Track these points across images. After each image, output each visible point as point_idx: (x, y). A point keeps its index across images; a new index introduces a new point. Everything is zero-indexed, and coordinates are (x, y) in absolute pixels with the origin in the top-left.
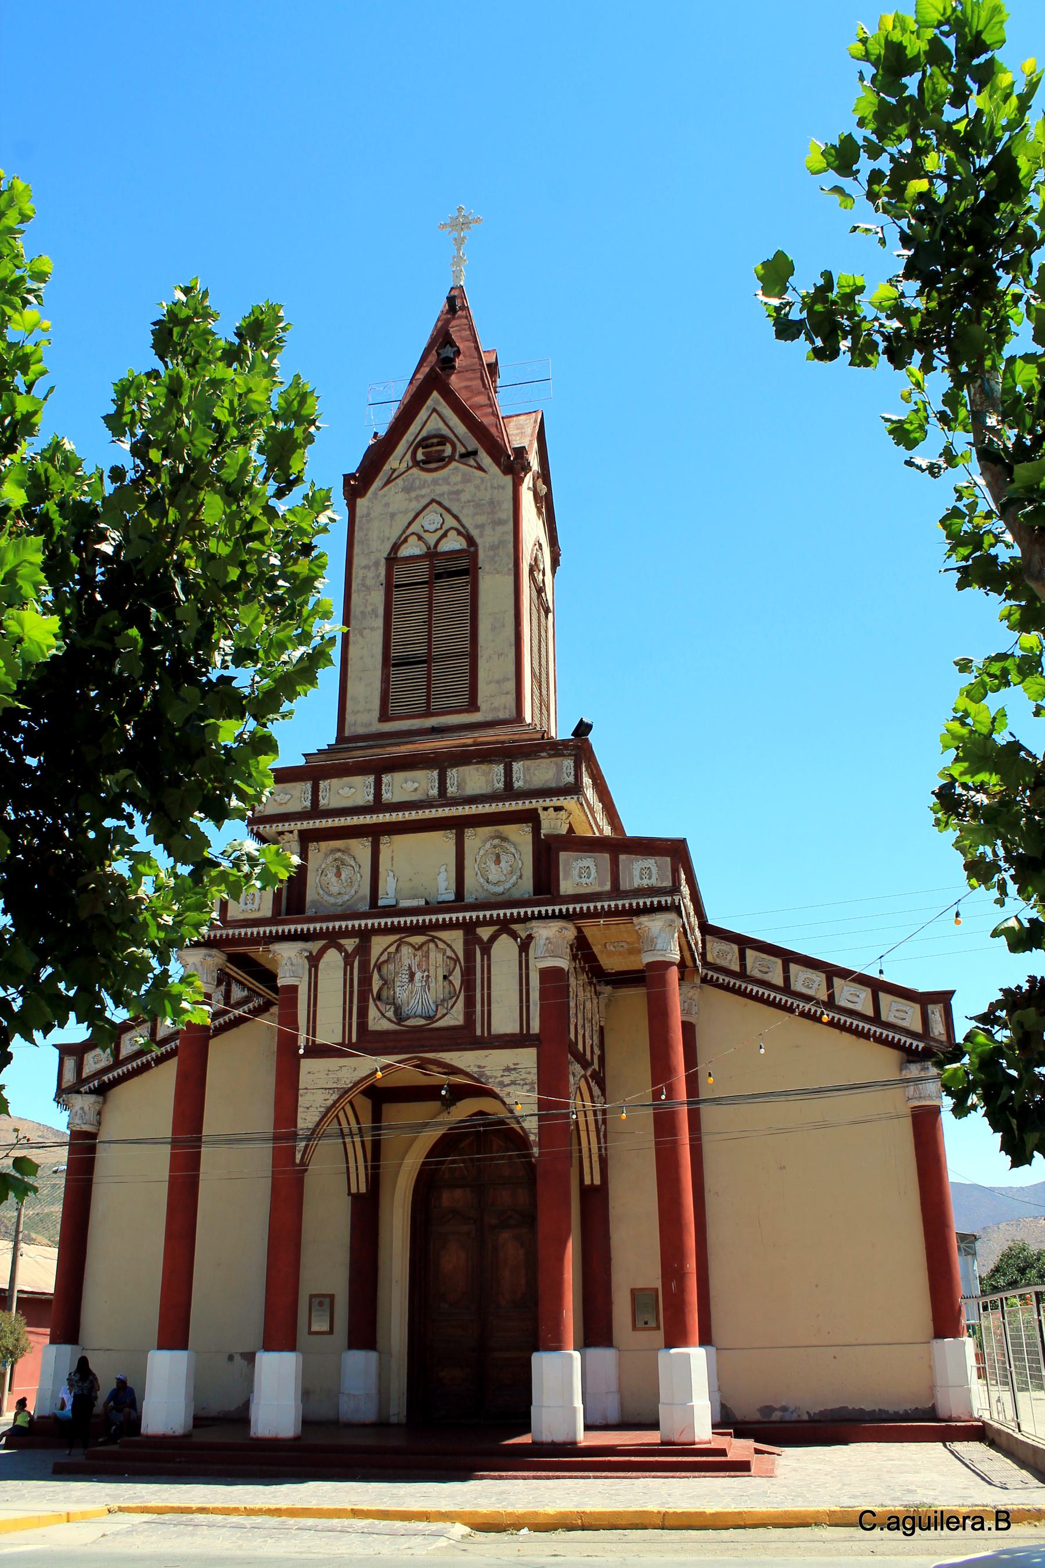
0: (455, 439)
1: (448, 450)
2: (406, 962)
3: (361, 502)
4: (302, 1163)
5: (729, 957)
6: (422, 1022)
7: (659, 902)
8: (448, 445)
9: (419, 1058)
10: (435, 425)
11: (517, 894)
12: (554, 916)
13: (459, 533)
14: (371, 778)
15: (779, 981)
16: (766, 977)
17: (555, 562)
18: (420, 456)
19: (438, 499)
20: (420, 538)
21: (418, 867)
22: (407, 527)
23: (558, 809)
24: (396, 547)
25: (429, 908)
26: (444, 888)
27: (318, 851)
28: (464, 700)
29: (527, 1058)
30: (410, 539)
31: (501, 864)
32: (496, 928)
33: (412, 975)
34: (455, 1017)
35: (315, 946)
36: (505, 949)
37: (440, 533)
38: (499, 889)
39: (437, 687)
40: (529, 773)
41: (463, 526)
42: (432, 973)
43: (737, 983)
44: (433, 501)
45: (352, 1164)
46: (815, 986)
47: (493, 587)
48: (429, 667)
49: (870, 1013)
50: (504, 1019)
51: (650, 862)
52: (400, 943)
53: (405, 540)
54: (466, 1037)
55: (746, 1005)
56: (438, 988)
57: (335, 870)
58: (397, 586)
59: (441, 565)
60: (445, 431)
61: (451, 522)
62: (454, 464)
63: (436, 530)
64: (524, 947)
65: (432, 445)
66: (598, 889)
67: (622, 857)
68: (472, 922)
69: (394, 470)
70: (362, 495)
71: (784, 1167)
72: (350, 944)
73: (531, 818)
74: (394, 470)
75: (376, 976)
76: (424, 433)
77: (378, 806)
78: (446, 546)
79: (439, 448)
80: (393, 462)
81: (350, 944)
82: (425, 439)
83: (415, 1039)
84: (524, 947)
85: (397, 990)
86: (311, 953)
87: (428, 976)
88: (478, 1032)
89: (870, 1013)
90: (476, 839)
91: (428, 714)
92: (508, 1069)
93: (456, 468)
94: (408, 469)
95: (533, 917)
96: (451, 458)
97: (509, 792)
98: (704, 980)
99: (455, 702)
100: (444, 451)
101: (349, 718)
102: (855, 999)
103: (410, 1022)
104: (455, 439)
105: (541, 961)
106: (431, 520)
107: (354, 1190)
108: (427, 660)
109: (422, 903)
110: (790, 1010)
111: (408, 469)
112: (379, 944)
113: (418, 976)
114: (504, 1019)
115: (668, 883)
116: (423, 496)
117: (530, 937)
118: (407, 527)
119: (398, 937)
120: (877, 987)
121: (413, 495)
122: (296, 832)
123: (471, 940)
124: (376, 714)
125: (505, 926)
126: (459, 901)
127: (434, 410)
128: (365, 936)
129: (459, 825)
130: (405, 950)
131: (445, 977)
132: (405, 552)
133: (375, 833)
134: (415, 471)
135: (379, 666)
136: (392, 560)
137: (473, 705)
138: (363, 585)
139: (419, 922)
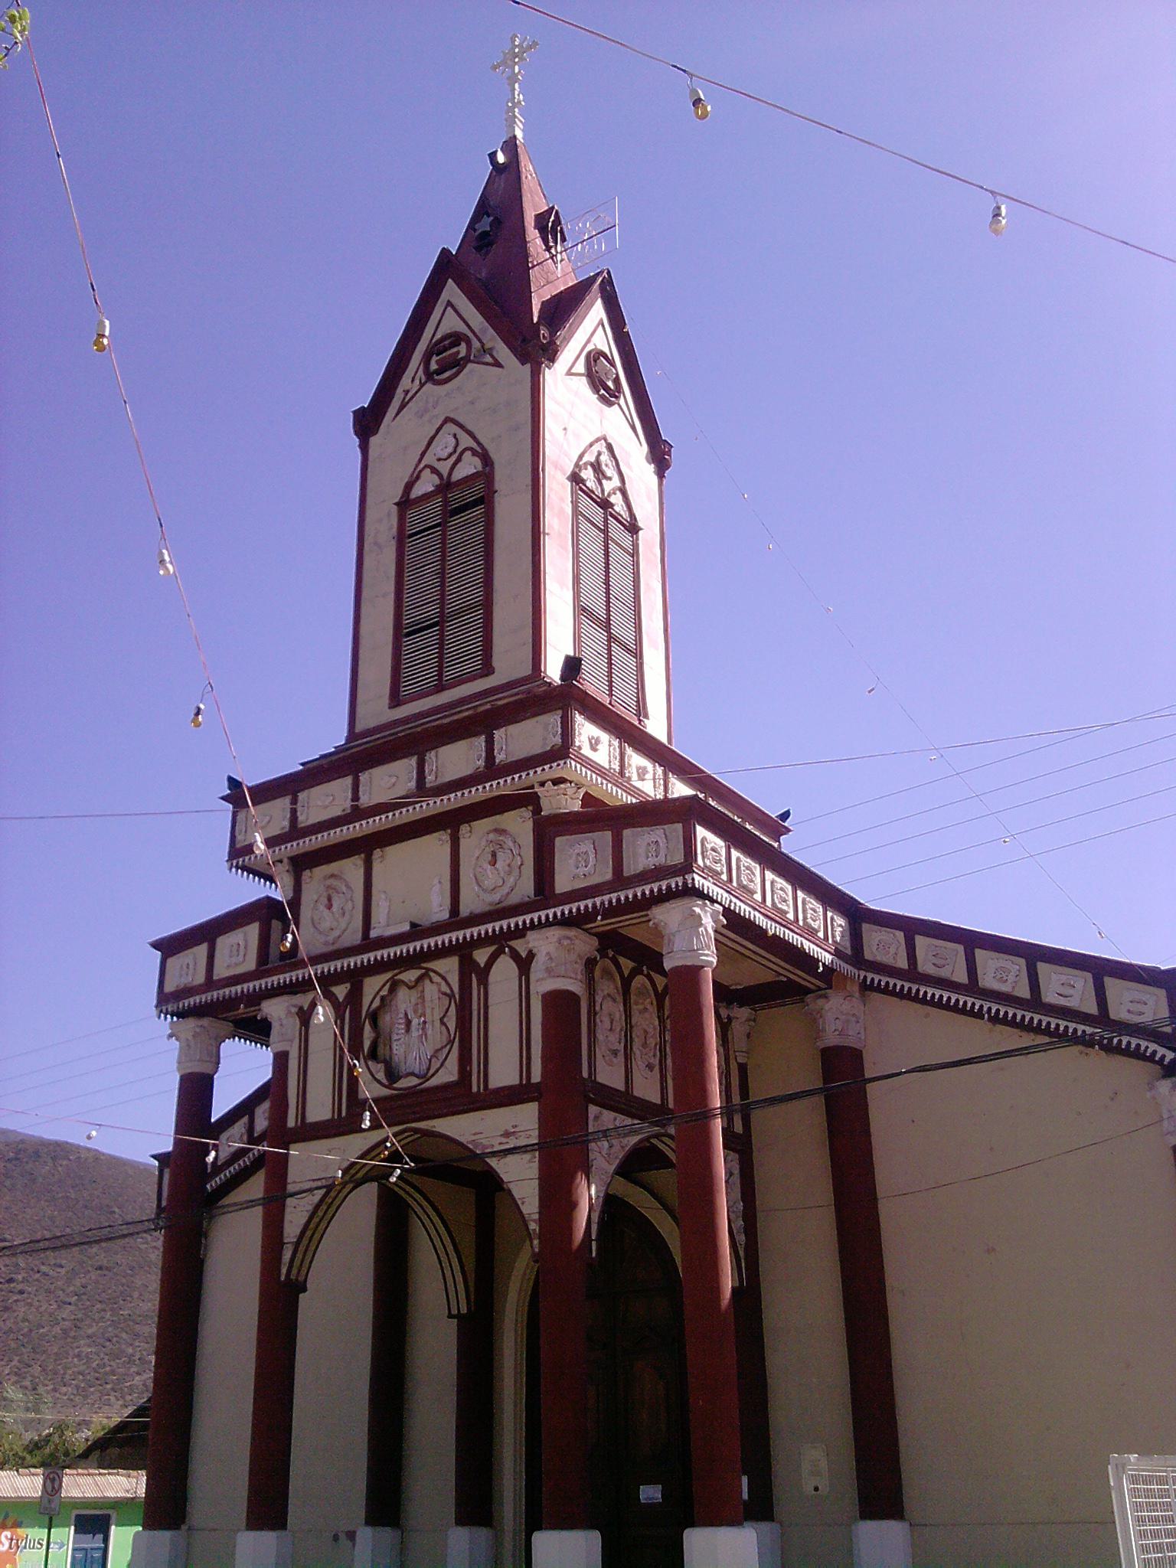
0: (470, 334)
1: (462, 349)
2: (402, 1007)
3: (374, 440)
4: (749, 1293)
5: (892, 950)
6: (414, 1081)
7: (669, 887)
8: (463, 345)
9: (416, 1131)
10: (451, 324)
11: (514, 899)
12: (548, 924)
13: (474, 453)
14: (608, 835)
15: (962, 977)
16: (944, 973)
17: (660, 455)
18: (434, 366)
19: (452, 416)
20: (434, 471)
21: (411, 884)
22: (420, 461)
23: (557, 782)
24: (409, 486)
25: (417, 931)
26: (438, 909)
27: (315, 880)
28: (476, 665)
29: (525, 1119)
30: (423, 474)
31: (497, 866)
32: (493, 948)
33: (408, 1023)
34: (449, 1074)
35: (304, 1000)
36: (504, 972)
37: (454, 458)
38: (496, 897)
39: (450, 649)
40: (518, 740)
41: (479, 443)
42: (429, 1018)
43: (908, 984)
44: (447, 420)
45: (448, 1273)
46: (1011, 978)
47: (509, 510)
48: (442, 631)
49: (1092, 1009)
50: (504, 1072)
51: (657, 834)
52: (394, 985)
53: (418, 478)
54: (464, 1096)
55: (927, 1016)
56: (436, 1036)
57: (326, 901)
58: (411, 536)
59: (456, 497)
60: (462, 328)
61: (466, 441)
62: (470, 366)
63: (450, 455)
64: (524, 964)
65: (445, 350)
66: (596, 880)
67: (627, 833)
68: (469, 944)
69: (407, 392)
70: (375, 432)
71: (994, 1249)
72: (341, 991)
73: (528, 800)
74: (407, 392)
75: (367, 1027)
76: (438, 336)
77: (358, 813)
78: (460, 473)
79: (455, 350)
80: (405, 382)
81: (341, 991)
82: (436, 343)
83: (408, 1105)
84: (524, 964)
85: (394, 1047)
86: (301, 1008)
87: (425, 1022)
88: (475, 1089)
89: (1092, 1009)
90: (475, 837)
91: (440, 688)
92: (507, 1134)
93: (471, 371)
94: (422, 385)
95: (533, 927)
96: (467, 360)
97: (492, 770)
98: (866, 987)
99: (468, 668)
100: (458, 353)
101: (360, 710)
102: (1071, 991)
103: (403, 1083)
104: (470, 334)
105: (542, 984)
106: (444, 445)
107: (455, 1312)
108: (441, 622)
109: (406, 927)
110: (979, 1015)
111: (422, 385)
112: (373, 987)
113: (415, 1022)
114: (504, 1072)
115: (678, 858)
116: (436, 416)
117: (531, 955)
118: (420, 461)
119: (389, 975)
120: (1100, 970)
121: (426, 417)
122: (286, 861)
123: (468, 966)
124: (386, 700)
125: (501, 941)
126: (455, 921)
127: (449, 304)
128: (355, 977)
129: (451, 822)
130: (402, 993)
131: (441, 1020)
132: (417, 491)
133: (366, 847)
134: (429, 386)
135: (390, 639)
136: (405, 504)
137: (487, 669)
138: (376, 543)
139: (411, 954)
